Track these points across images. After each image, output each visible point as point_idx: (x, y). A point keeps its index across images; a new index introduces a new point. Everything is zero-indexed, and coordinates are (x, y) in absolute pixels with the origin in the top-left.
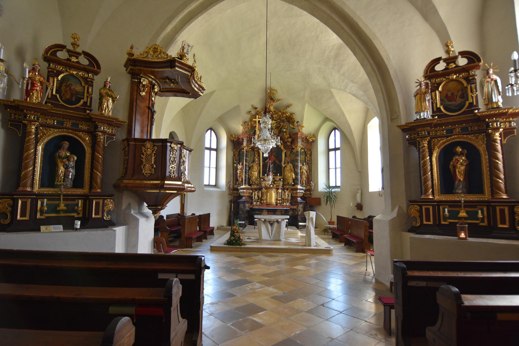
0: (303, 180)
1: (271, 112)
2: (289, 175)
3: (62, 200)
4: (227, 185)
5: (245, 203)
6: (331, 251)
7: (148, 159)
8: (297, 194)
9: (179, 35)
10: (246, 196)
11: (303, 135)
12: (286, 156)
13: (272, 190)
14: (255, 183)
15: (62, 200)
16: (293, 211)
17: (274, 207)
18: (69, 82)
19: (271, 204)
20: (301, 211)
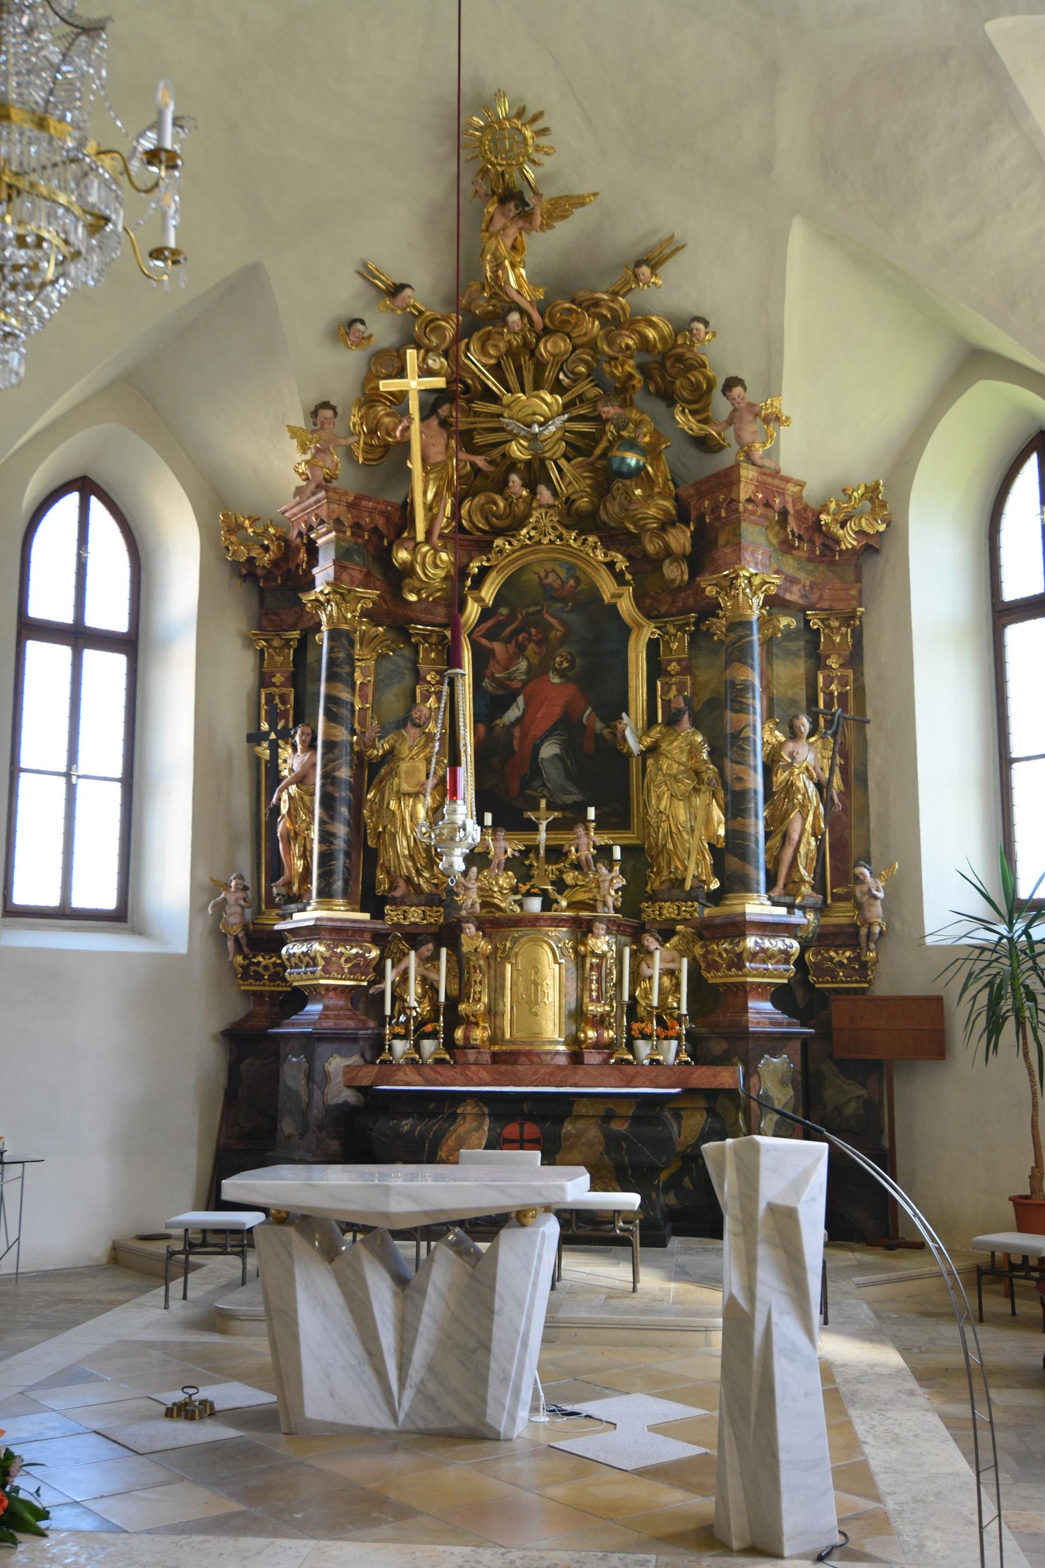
0: (797, 850)
1: (514, 317)
2: (682, 815)
4: (196, 908)
5: (322, 1048)
8: (741, 966)
10: (327, 987)
11: (782, 493)
12: (656, 669)
13: (537, 942)
14: (417, 888)
16: (710, 1111)
17: (556, 1075)
19: (528, 1054)
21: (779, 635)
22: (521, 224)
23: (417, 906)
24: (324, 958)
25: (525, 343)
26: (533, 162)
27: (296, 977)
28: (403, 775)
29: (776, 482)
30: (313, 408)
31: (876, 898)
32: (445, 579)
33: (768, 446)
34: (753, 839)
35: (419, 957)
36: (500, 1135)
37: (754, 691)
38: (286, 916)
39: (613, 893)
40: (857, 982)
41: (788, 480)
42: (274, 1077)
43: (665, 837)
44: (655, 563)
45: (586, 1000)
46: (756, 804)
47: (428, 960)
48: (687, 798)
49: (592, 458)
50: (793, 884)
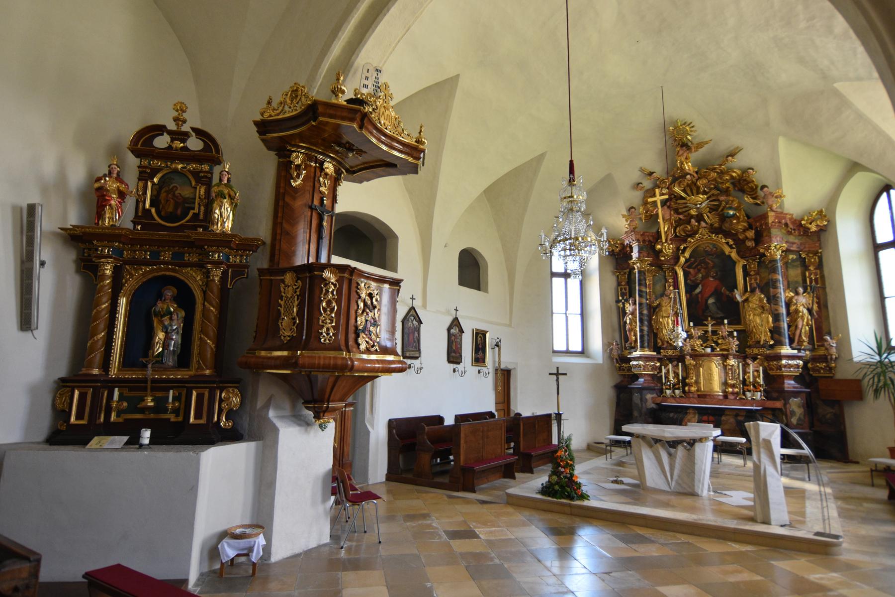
0: (801, 331)
3: (149, 390)
4: (604, 350)
5: (644, 392)
6: (835, 549)
7: (288, 307)
8: (781, 369)
9: (358, 55)
10: (645, 374)
11: (785, 218)
12: (746, 274)
13: (711, 361)
15: (149, 390)
17: (719, 402)
18: (172, 184)
19: (709, 395)
20: (798, 415)
21: (790, 261)
22: (688, 152)
23: (671, 350)
24: (643, 366)
25: (693, 182)
26: (690, 135)
27: (635, 371)
28: (663, 312)
29: (782, 215)
30: (628, 209)
31: (832, 346)
32: (672, 253)
33: (778, 205)
34: (783, 329)
35: (672, 365)
36: (701, 419)
37: (779, 282)
38: (631, 353)
39: (734, 346)
40: (828, 374)
41: (786, 214)
42: (631, 400)
43: (752, 327)
44: (743, 241)
45: (728, 379)
46: (783, 317)
47: (675, 366)
48: (760, 315)
49: (718, 212)
50: (800, 342)
